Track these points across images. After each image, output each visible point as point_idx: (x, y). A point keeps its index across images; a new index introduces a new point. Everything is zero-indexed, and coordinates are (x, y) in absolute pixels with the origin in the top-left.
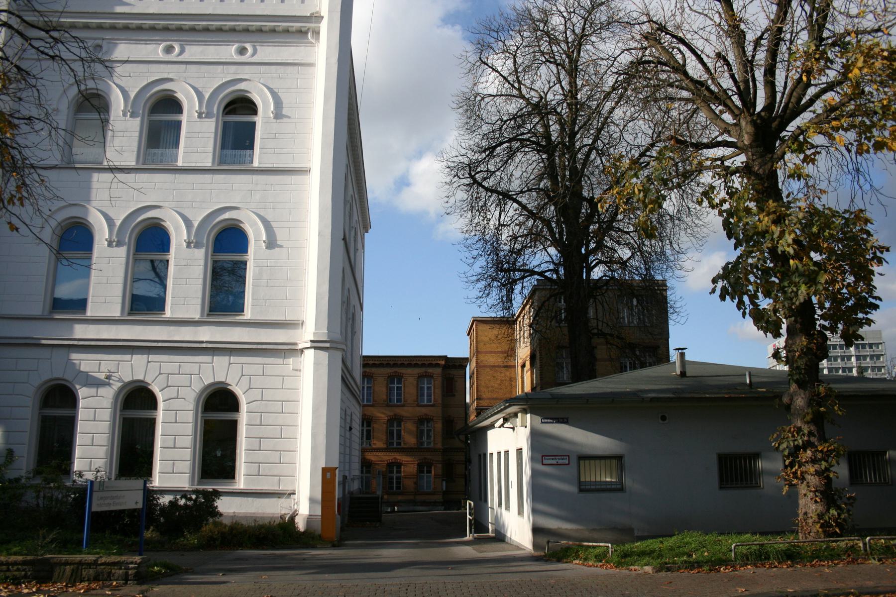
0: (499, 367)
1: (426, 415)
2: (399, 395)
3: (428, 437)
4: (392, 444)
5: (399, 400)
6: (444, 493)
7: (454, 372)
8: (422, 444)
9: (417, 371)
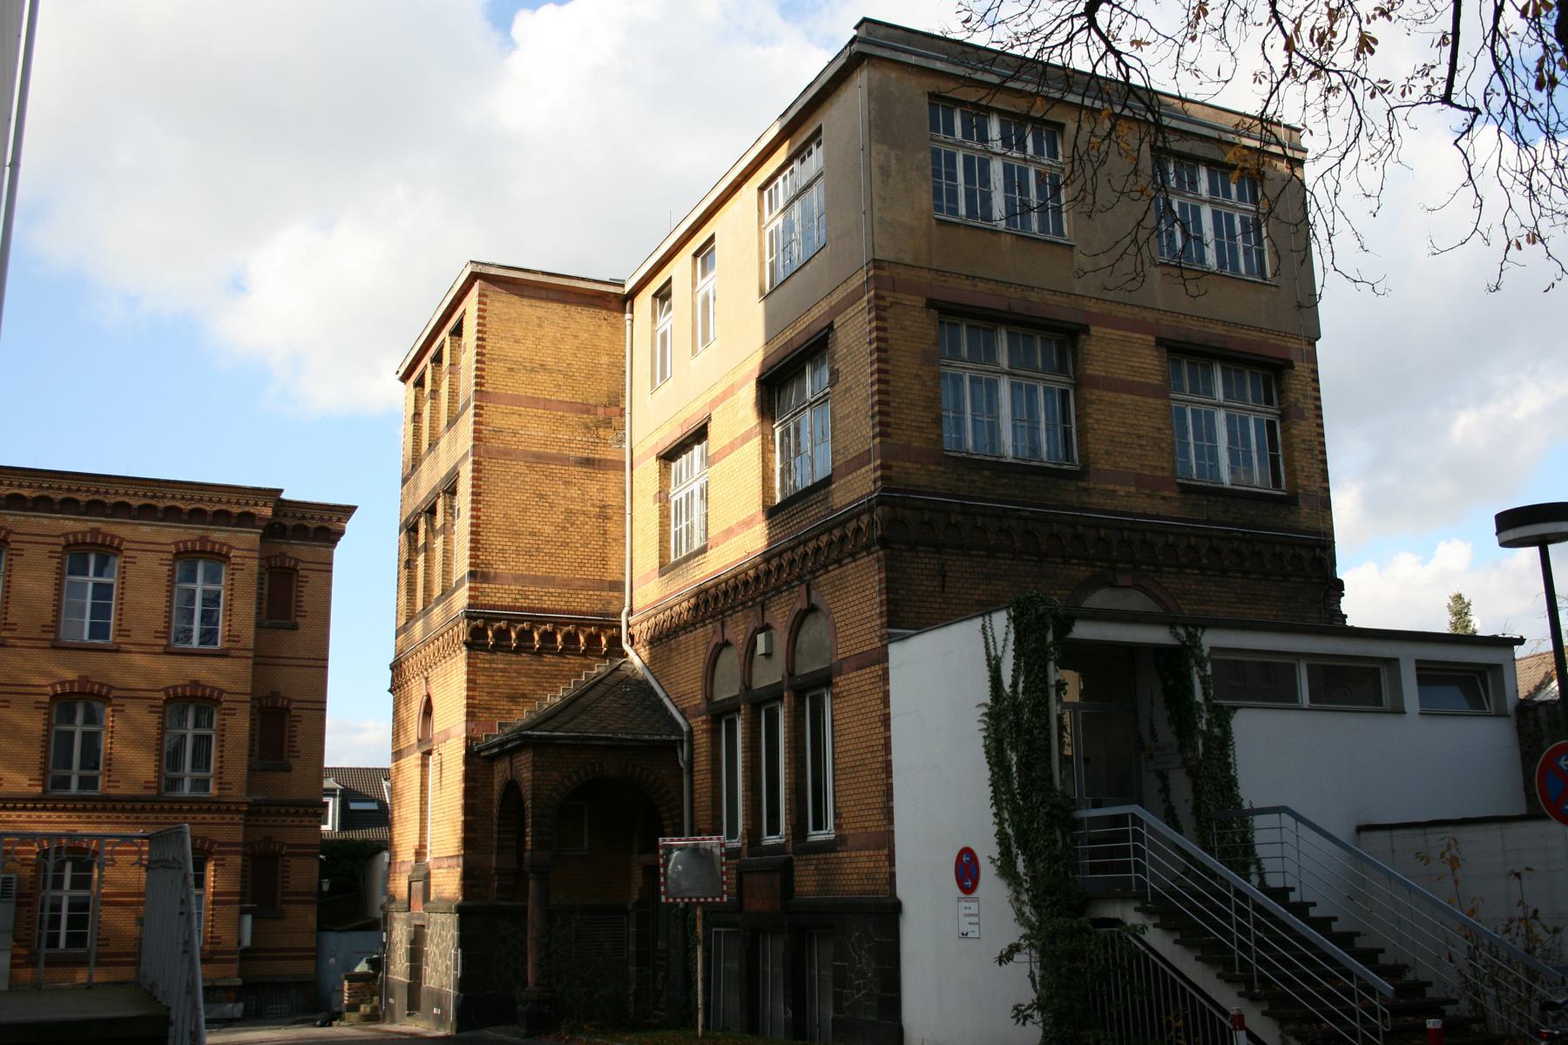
0: (562, 460)
1: (195, 684)
2: (100, 611)
3: (201, 760)
4: (65, 782)
5: (99, 630)
6: (246, 955)
7: (302, 551)
8: (175, 783)
9: (172, 535)
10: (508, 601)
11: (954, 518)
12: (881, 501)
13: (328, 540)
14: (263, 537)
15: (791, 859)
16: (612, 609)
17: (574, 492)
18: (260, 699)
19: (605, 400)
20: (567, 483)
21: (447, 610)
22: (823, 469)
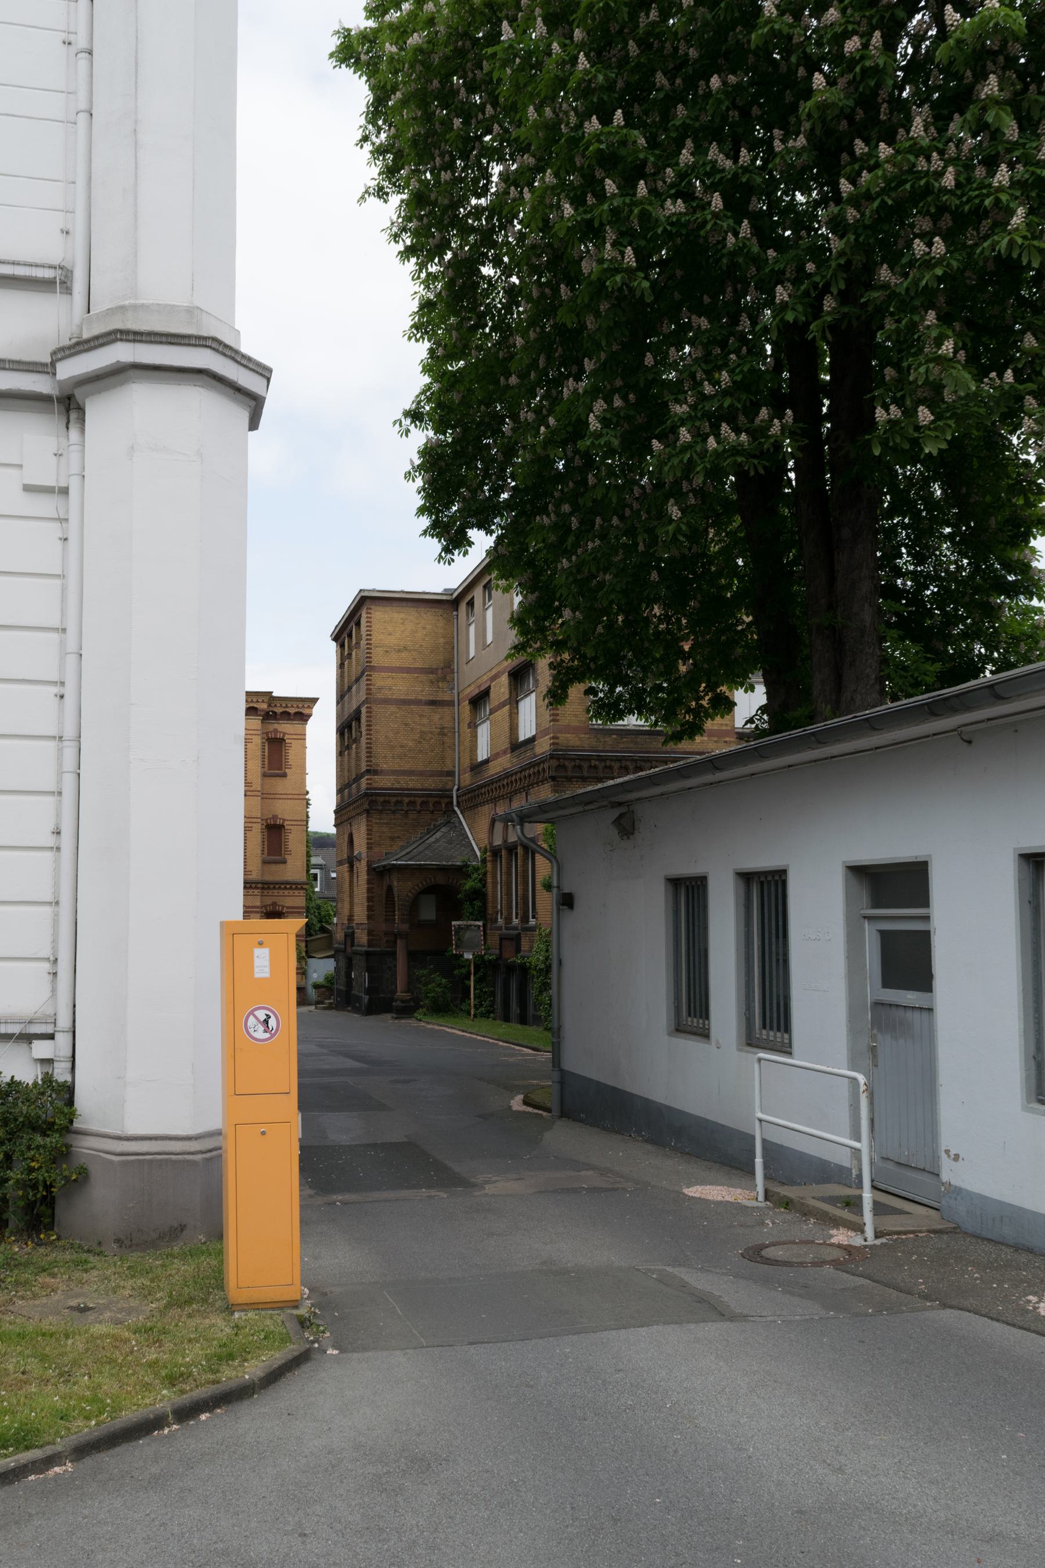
7: (285, 728)
10: (389, 785)
11: (593, 763)
12: (552, 757)
13: (302, 720)
14: (263, 721)
15: (519, 934)
16: (448, 787)
17: (425, 721)
18: (266, 820)
19: (442, 665)
20: (421, 716)
21: (358, 788)
22: (534, 733)
